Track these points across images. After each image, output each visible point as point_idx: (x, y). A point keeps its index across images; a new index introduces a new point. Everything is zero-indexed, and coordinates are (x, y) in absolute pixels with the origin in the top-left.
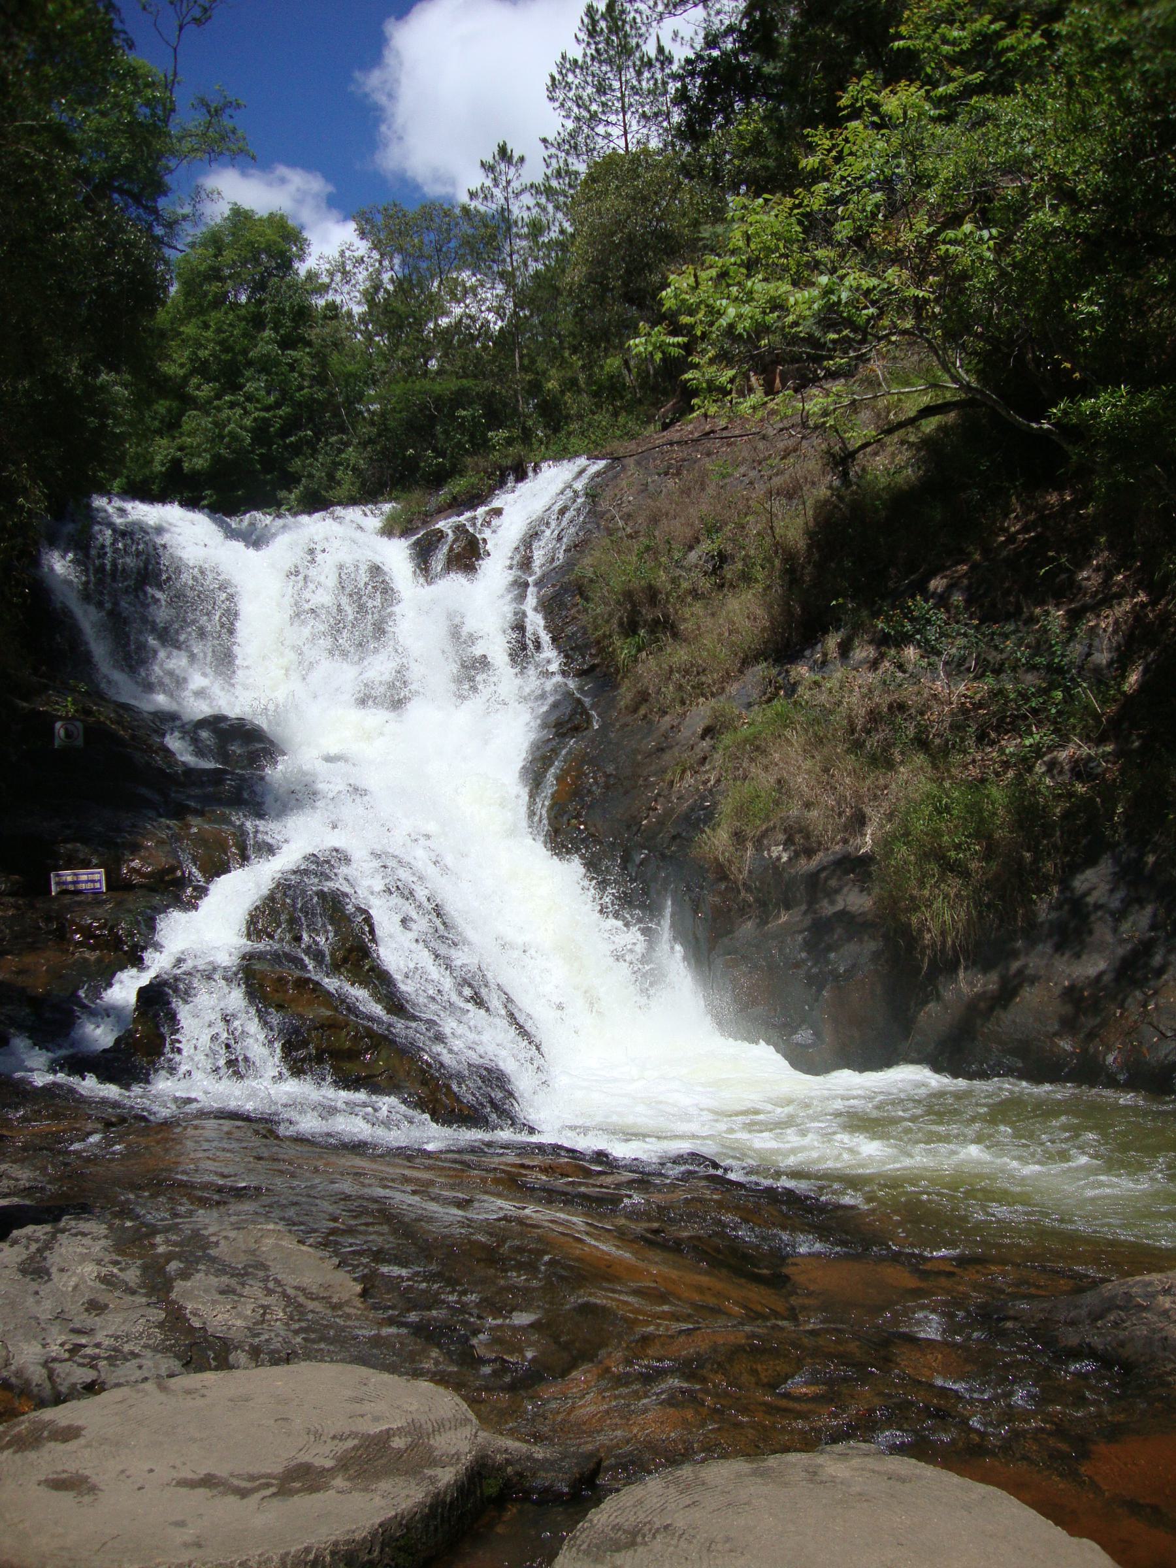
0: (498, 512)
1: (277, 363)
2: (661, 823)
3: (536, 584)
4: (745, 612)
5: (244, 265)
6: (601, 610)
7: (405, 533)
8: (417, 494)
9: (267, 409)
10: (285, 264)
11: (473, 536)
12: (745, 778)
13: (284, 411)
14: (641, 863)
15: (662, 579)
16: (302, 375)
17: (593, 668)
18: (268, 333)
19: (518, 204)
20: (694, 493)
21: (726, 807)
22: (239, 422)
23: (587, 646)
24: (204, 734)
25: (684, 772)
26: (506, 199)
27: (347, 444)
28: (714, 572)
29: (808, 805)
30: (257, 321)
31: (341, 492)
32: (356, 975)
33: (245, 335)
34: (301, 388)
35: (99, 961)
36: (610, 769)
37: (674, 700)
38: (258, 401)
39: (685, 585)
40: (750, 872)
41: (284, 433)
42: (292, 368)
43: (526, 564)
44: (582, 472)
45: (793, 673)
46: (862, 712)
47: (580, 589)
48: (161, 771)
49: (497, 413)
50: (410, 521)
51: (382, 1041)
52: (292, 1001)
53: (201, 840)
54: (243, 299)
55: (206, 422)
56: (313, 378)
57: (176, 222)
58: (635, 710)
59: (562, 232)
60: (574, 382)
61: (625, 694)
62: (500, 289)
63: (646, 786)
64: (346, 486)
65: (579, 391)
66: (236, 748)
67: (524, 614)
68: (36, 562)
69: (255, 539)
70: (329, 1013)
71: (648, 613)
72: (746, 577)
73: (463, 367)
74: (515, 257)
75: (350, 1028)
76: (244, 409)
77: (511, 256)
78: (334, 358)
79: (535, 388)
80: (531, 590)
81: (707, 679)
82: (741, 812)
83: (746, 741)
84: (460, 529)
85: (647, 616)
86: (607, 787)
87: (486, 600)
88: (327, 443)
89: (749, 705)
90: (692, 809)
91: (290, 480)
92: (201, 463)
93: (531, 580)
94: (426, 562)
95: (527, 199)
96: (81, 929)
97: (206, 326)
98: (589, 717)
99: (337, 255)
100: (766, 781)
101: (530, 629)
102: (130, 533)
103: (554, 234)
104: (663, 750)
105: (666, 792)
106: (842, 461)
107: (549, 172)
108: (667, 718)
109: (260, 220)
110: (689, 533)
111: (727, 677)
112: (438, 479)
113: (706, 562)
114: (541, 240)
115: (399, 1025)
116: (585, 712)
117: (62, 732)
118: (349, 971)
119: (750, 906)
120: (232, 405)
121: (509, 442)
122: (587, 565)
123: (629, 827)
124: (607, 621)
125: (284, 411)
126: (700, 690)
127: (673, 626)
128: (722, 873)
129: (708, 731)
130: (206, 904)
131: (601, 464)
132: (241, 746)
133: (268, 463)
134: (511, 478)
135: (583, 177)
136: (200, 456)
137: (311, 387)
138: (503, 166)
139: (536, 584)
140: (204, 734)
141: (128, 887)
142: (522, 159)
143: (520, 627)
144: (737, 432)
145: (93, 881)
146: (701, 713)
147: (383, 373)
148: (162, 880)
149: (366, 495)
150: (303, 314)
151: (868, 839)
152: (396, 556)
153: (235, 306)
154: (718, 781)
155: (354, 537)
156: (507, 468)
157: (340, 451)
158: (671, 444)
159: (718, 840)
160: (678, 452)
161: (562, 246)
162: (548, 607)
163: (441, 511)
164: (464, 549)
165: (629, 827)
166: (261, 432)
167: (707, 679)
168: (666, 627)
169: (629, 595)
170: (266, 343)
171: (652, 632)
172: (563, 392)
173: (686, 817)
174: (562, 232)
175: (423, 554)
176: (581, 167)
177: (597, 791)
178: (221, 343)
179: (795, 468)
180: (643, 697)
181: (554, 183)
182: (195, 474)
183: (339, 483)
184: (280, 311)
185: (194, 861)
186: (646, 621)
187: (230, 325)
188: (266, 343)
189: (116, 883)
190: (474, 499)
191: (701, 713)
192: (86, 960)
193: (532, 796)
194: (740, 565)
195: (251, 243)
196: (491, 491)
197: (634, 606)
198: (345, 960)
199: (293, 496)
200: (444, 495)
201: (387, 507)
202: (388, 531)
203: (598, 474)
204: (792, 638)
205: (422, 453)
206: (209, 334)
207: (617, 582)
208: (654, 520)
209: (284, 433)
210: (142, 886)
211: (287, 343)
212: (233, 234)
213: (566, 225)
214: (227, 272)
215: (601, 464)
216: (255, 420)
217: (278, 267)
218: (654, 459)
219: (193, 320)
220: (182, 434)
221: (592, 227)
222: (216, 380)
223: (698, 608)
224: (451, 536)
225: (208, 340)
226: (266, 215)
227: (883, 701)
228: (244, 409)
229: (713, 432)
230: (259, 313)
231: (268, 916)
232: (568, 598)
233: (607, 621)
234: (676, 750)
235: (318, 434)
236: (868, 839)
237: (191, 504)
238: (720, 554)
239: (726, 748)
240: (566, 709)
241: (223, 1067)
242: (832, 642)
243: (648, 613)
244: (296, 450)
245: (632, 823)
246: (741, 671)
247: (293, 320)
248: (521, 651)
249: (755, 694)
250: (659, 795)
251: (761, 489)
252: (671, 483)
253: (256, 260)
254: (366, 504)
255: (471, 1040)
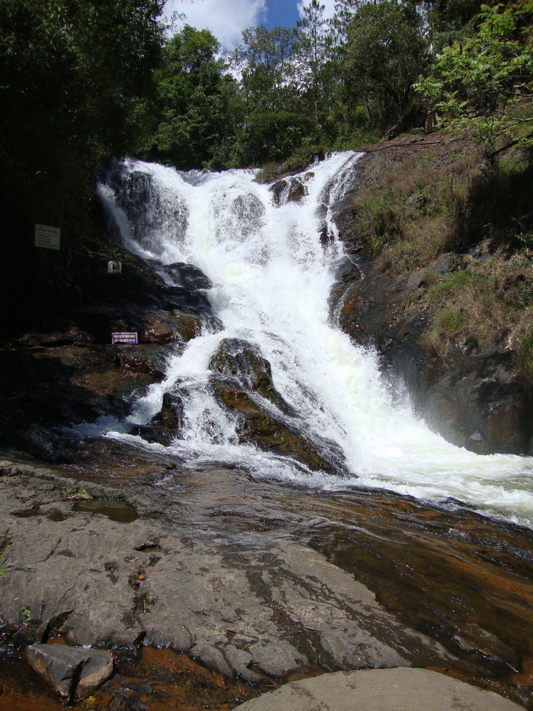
0: (312, 174)
1: (204, 101)
2: (399, 326)
3: (332, 208)
4: (437, 228)
5: (190, 54)
6: (365, 222)
7: (267, 182)
8: (271, 165)
9: (199, 122)
10: (209, 56)
11: (301, 185)
12: (443, 307)
13: (206, 124)
14: (389, 345)
15: (396, 209)
16: (215, 107)
17: (360, 250)
18: (200, 87)
19: (320, 29)
20: (409, 170)
21: (437, 320)
22: (184, 128)
23: (357, 240)
24: (174, 271)
25: (410, 302)
26: (315, 26)
27: (235, 141)
28: (420, 208)
29: (478, 323)
30: (195, 81)
31: (231, 163)
32: (265, 393)
33: (189, 87)
34: (214, 113)
35: (138, 377)
36: (372, 299)
37: (403, 268)
38: (194, 119)
39: (408, 213)
40: (448, 353)
41: (205, 135)
42: (210, 103)
43: (326, 200)
44: (350, 159)
45: (465, 258)
46: (503, 279)
47: (354, 212)
48: (159, 287)
49: (308, 128)
50: (269, 177)
51: (281, 426)
52: (237, 404)
53: (182, 321)
54: (188, 71)
55: (170, 127)
56: (220, 109)
57: (164, 29)
58: (384, 271)
59: (342, 43)
60: (341, 116)
61: (379, 263)
62: (310, 71)
63: (391, 308)
64: (234, 161)
65: (344, 121)
66: (190, 279)
67: (326, 223)
68: (95, 188)
69: (195, 182)
70: (256, 412)
71: (389, 225)
72: (437, 211)
73: (291, 107)
74: (317, 55)
75: (266, 419)
76: (188, 122)
77: (316, 54)
78: (231, 100)
79: (322, 120)
80: (329, 211)
81: (421, 258)
82: (445, 323)
83: (443, 289)
84: (294, 181)
85: (389, 227)
86: (370, 307)
87: (307, 215)
88: (226, 140)
89: (443, 272)
90: (415, 321)
91: (208, 157)
92: (166, 147)
93: (328, 207)
94: (278, 196)
95: (325, 27)
96: (129, 362)
97: (172, 82)
98: (359, 273)
99: (234, 51)
100: (455, 309)
101: (329, 230)
102: (138, 177)
103: (338, 44)
104: (399, 291)
105: (401, 312)
106: (491, 157)
107: (337, 13)
108: (400, 276)
109: (198, 32)
110: (408, 188)
111: (430, 258)
112: (279, 159)
113: (417, 202)
114: (331, 47)
115: (289, 420)
116: (357, 271)
117: (112, 266)
118: (261, 390)
119: (447, 370)
120: (182, 120)
121: (312, 143)
122: (358, 200)
123: (383, 327)
124: (369, 228)
125: (206, 124)
126: (417, 263)
127: (401, 233)
128: (434, 353)
129: (423, 284)
130: (186, 353)
131: (361, 154)
132: (192, 278)
133: (197, 148)
134: (317, 159)
135: (353, 16)
136: (166, 144)
137: (219, 113)
138: (314, 10)
139: (332, 208)
140: (174, 271)
141: (149, 342)
142: (323, 7)
143: (324, 230)
144: (429, 142)
145: (132, 338)
146: (418, 275)
147: (254, 108)
148: (164, 340)
149: (244, 164)
150: (216, 78)
151: (510, 341)
152: (264, 193)
153: (185, 74)
154: (428, 308)
155: (241, 182)
156: (315, 154)
157: (232, 144)
158: (397, 146)
159: (432, 336)
160: (400, 150)
161: (341, 51)
162: (338, 220)
163: (284, 172)
164: (297, 190)
165: (383, 327)
166: (194, 133)
167: (421, 258)
168: (397, 232)
169: (380, 216)
170: (199, 91)
171: (391, 234)
172: (335, 122)
173: (412, 325)
174: (342, 43)
175: (277, 190)
176: (353, 11)
177: (366, 309)
178: (178, 90)
179: (462, 158)
180: (388, 265)
181: (340, 19)
182: (164, 151)
183: (230, 159)
184: (206, 76)
185: (178, 330)
186: (388, 229)
187: (183, 82)
188: (199, 91)
189: (142, 340)
190: (300, 168)
191: (418, 275)
192: (131, 377)
193: (332, 309)
194: (434, 205)
195: (194, 44)
196: (307, 165)
197: (383, 221)
198: (259, 385)
199: (209, 164)
200: (284, 165)
201: (257, 170)
202: (259, 180)
203: (360, 159)
204: (462, 241)
205: (275, 144)
206: (173, 86)
207: (376, 209)
208: (390, 181)
209: (205, 135)
210: (155, 342)
211: (208, 92)
212: (186, 39)
213: (344, 39)
214: (181, 57)
215: (361, 154)
216: (192, 127)
217: (206, 56)
218: (388, 153)
219: (166, 79)
220: (158, 133)
221: (360, 40)
222: (175, 108)
223: (413, 223)
224: (290, 184)
225: (172, 89)
226: (201, 31)
227: (514, 275)
228: (188, 122)
229: (416, 141)
230: (196, 78)
231: (219, 360)
232: (347, 216)
233: (369, 228)
234: (406, 291)
235: (222, 136)
236: (510, 341)
237: (164, 163)
238: (424, 199)
239: (433, 292)
240: (348, 269)
241: (207, 437)
242: (485, 244)
243: (389, 225)
244: (211, 142)
245: (384, 326)
246: (437, 255)
247: (212, 81)
248: (325, 239)
249: (446, 268)
250: (397, 313)
251: (443, 168)
252: (398, 165)
253: (196, 52)
254: (245, 168)
255: (320, 427)
